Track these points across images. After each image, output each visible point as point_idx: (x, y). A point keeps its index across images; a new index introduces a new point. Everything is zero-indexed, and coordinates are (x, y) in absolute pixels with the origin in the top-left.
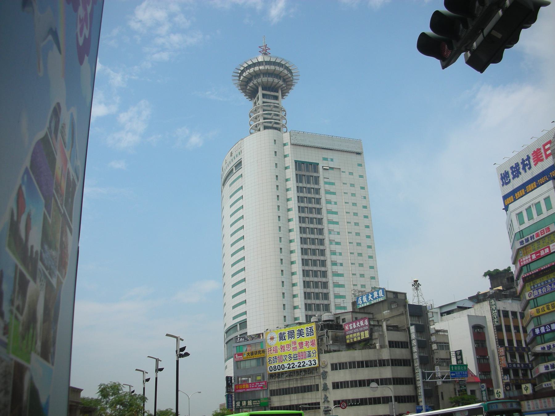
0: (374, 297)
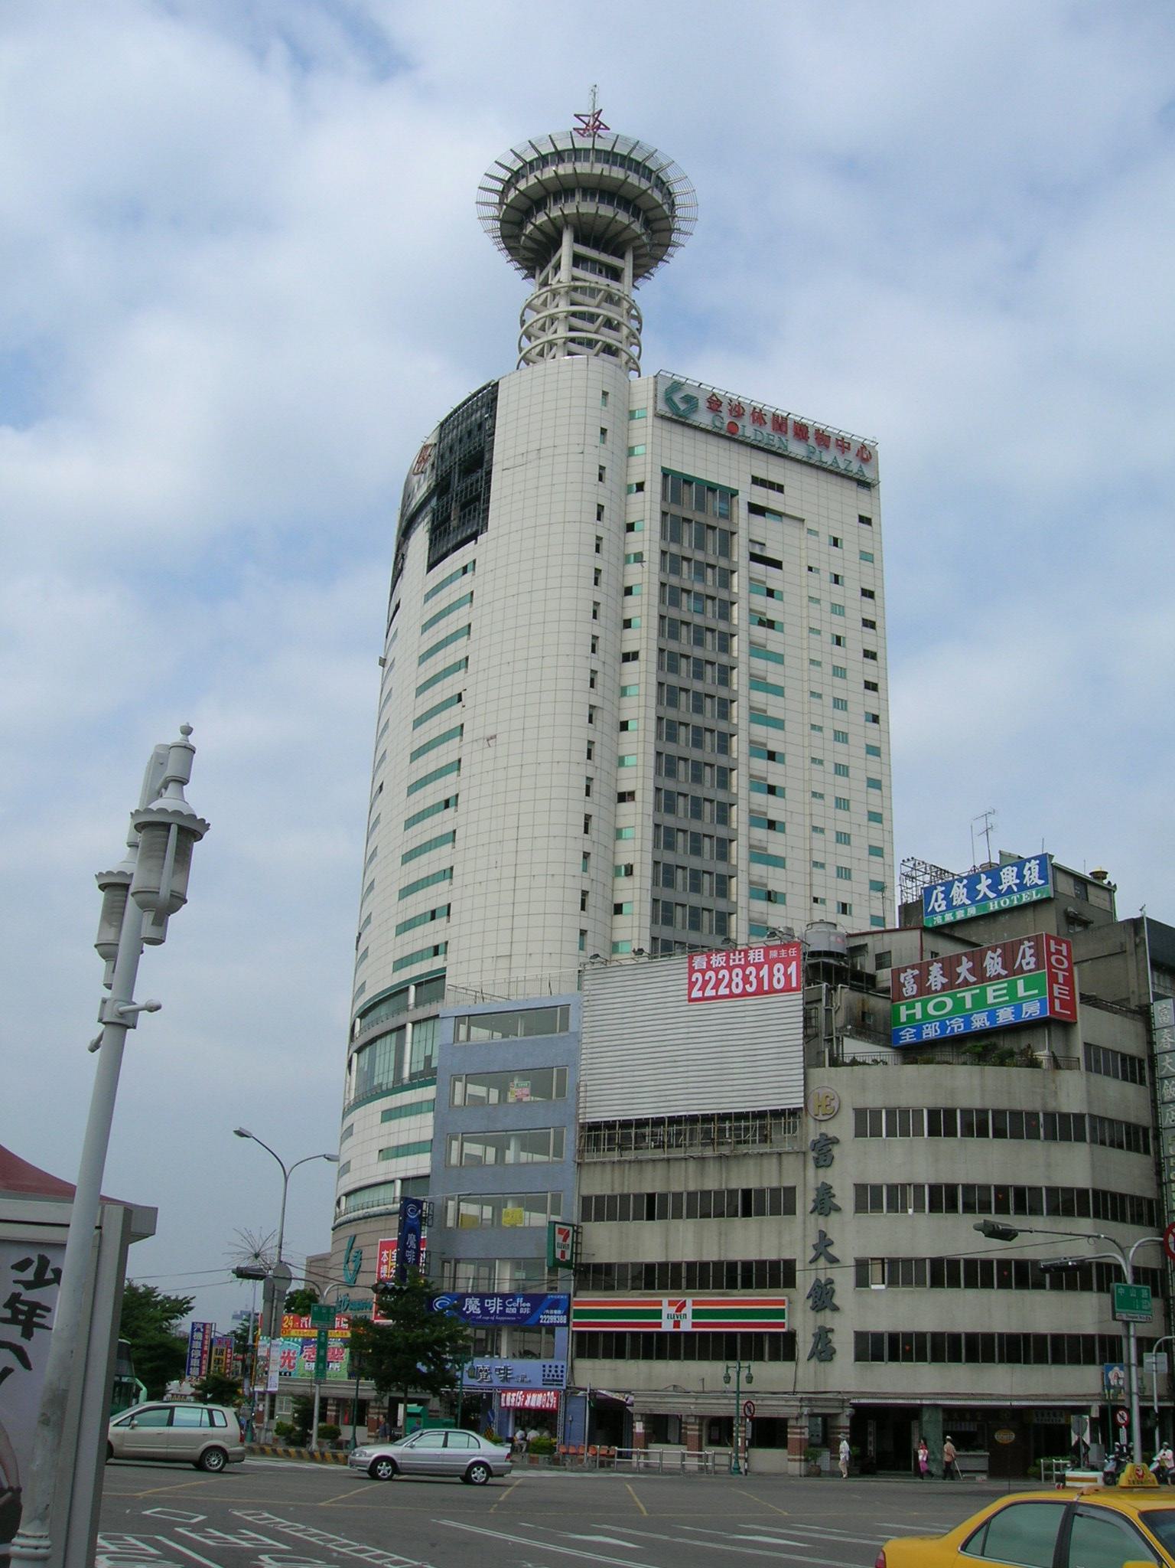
0: (1004, 887)
